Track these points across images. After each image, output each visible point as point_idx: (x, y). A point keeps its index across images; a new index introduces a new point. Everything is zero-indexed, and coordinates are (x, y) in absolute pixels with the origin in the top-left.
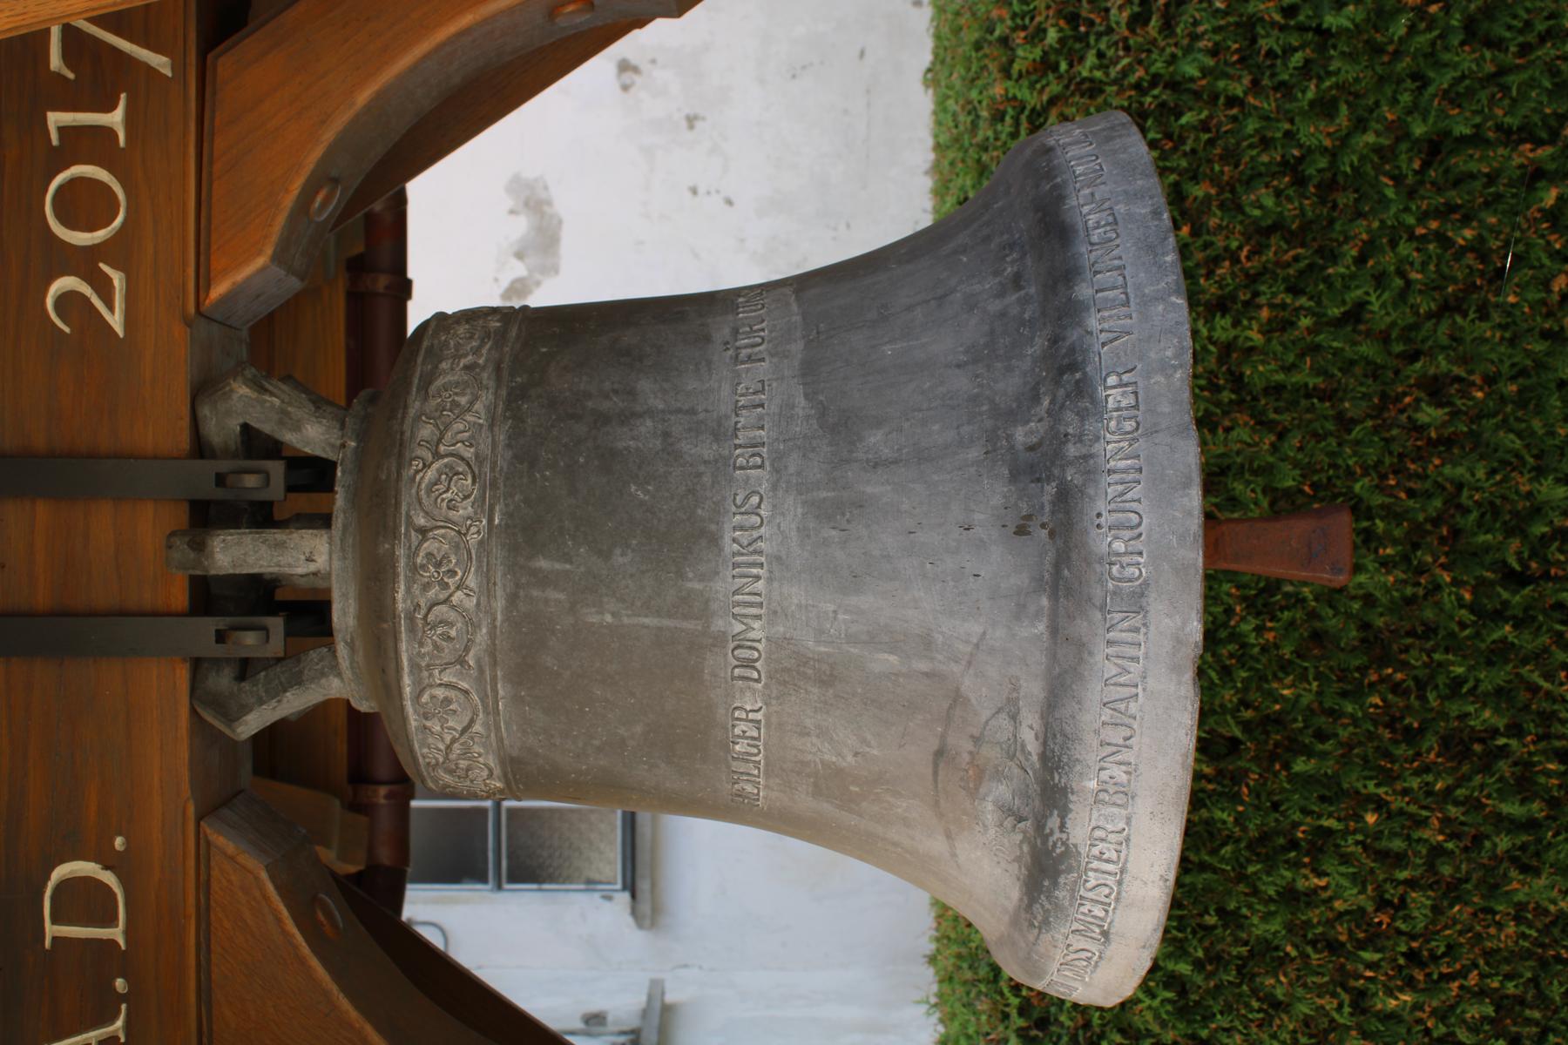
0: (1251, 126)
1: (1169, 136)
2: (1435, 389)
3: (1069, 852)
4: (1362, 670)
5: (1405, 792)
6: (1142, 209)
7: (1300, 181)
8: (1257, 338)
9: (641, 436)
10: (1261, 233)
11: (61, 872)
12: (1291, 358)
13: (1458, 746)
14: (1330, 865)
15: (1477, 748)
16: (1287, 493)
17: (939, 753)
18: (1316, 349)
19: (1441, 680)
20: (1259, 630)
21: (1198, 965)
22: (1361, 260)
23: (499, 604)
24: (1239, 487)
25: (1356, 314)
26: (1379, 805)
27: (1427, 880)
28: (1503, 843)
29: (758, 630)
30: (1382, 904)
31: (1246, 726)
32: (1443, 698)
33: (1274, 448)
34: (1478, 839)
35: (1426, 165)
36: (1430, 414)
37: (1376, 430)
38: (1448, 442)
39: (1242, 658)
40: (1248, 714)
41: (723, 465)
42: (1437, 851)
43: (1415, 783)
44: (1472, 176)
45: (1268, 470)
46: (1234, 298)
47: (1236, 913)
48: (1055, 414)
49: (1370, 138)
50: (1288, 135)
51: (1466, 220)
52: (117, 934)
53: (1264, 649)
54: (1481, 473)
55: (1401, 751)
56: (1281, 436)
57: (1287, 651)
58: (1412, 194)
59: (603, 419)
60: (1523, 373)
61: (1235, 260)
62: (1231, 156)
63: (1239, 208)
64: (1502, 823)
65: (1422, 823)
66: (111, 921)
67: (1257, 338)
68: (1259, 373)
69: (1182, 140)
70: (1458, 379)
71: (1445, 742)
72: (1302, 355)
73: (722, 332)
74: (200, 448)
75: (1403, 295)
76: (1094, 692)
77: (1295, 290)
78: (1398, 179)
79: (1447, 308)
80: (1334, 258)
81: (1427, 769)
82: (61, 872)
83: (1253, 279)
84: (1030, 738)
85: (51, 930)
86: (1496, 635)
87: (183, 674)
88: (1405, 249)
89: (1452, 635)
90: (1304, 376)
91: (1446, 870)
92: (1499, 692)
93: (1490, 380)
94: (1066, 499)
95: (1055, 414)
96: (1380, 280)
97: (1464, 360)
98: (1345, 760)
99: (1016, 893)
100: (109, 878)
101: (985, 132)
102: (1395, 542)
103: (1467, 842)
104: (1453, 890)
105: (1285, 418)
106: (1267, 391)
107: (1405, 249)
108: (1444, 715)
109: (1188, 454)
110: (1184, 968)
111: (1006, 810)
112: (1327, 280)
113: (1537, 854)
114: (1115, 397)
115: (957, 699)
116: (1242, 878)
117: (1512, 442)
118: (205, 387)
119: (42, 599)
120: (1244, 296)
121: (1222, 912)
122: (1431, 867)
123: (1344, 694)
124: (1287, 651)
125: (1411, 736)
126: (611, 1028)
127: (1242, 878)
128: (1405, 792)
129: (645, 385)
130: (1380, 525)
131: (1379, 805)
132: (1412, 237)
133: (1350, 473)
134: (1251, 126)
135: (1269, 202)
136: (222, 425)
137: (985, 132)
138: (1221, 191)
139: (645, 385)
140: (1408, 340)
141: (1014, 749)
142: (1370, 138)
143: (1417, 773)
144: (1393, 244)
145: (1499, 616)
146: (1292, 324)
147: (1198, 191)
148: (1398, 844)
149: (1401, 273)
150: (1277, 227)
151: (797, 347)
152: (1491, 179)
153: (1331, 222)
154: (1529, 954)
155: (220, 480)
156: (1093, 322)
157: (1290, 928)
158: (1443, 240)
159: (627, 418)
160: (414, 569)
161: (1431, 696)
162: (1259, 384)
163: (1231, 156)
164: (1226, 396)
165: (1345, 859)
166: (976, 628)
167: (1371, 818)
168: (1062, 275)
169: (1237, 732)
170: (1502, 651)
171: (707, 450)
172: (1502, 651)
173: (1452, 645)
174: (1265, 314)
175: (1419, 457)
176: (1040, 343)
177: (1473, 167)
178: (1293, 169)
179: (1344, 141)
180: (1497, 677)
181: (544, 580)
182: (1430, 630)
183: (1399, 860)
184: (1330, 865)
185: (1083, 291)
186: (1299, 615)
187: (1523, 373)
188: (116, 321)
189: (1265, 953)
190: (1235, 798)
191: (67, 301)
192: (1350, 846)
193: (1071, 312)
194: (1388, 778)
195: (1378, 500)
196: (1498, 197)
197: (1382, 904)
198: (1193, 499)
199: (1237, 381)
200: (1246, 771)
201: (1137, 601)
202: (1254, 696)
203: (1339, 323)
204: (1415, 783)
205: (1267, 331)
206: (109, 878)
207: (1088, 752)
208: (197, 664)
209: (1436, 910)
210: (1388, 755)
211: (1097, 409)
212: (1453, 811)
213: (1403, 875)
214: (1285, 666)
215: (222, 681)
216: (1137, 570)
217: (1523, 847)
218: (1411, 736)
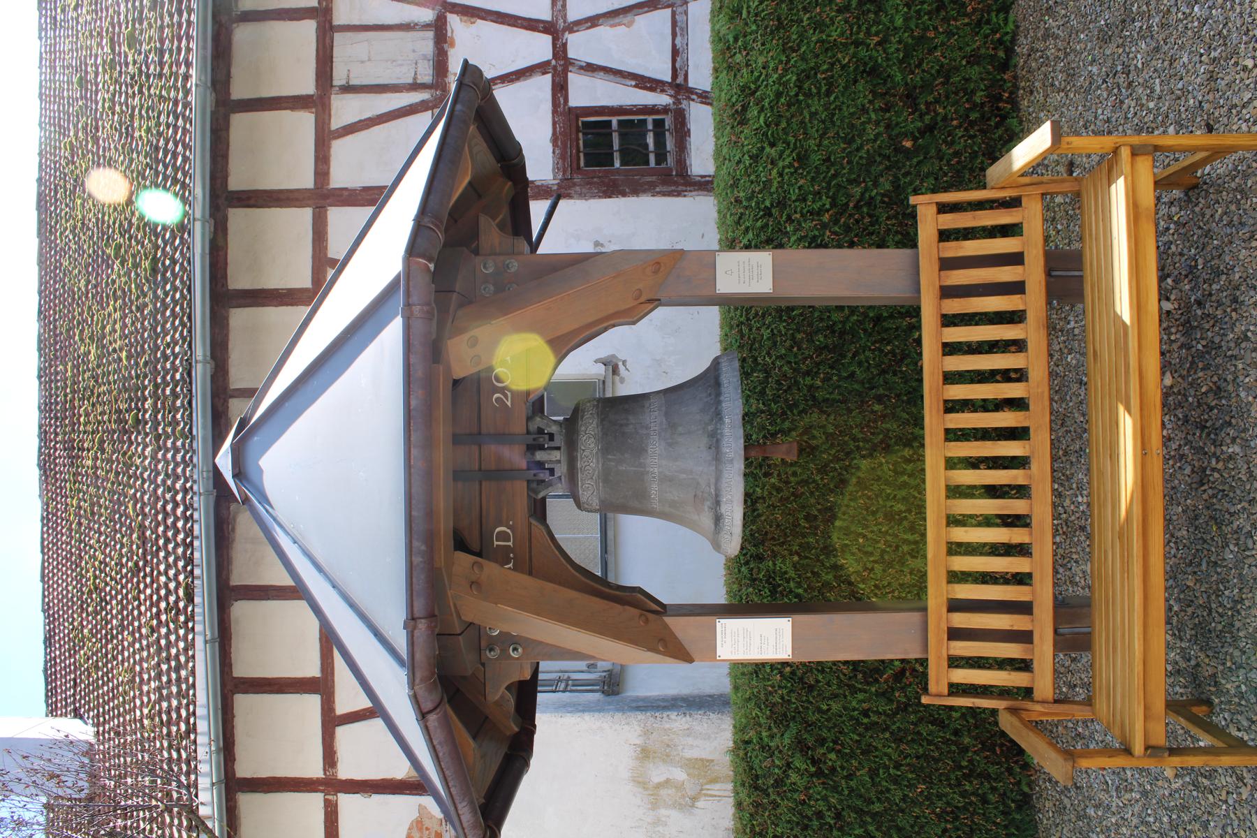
0: (816, 314)
1: (790, 318)
2: (879, 399)
3: (722, 515)
4: (857, 492)
5: (872, 532)
6: (735, 380)
7: (833, 332)
8: (819, 383)
9: (630, 429)
10: (820, 350)
11: (498, 529)
12: (831, 390)
13: (890, 516)
14: (848, 556)
15: (897, 517)
16: (831, 434)
17: (695, 496)
18: (839, 387)
19: (884, 494)
20: (822, 479)
21: (805, 590)
22: (854, 356)
23: (600, 465)
24: (815, 432)
25: (852, 374)
26: (864, 536)
27: (881, 561)
28: (906, 548)
29: (656, 470)
30: (866, 569)
31: (819, 511)
32: (884, 501)
33: (826, 419)
34: (897, 547)
35: (874, 326)
36: (877, 407)
37: (860, 413)
38: (884, 416)
39: (817, 488)
40: (819, 507)
41: (648, 435)
42: (883, 551)
43: (875, 529)
44: (891, 329)
45: (824, 427)
46: (811, 370)
47: (817, 573)
48: (716, 424)
49: (855, 318)
50: (829, 317)
51: (888, 344)
52: (510, 544)
53: (824, 485)
54: (895, 426)
55: (870, 518)
56: (828, 415)
57: (832, 486)
58: (870, 335)
59: (621, 425)
60: (909, 393)
61: (812, 358)
62: (810, 325)
63: (813, 341)
64: (906, 541)
65: (878, 542)
66: (509, 541)
67: (819, 383)
68: (820, 395)
69: (793, 319)
70: (887, 396)
71: (886, 515)
72: (834, 389)
73: (647, 405)
74: (528, 432)
75: (868, 368)
76: (724, 480)
77: (832, 368)
78: (865, 330)
79: (884, 372)
80: (844, 357)
81: (880, 524)
82: (498, 529)
83: (818, 364)
84: (712, 491)
85: (496, 543)
86: (902, 479)
87: (525, 483)
88: (867, 353)
89: (887, 480)
90: (836, 396)
91: (886, 557)
92: (904, 498)
93: (898, 396)
94: (718, 441)
95: (716, 424)
96: (860, 364)
97: (890, 389)
98: (852, 522)
99: (713, 526)
100: (509, 531)
101: (732, 314)
102: (867, 449)
103: (893, 548)
104: (890, 564)
105: (829, 410)
106: (824, 401)
107: (867, 353)
108: (885, 506)
109: (741, 432)
110: (800, 591)
111: (709, 507)
112: (842, 364)
113: (918, 552)
114: (727, 421)
115: (698, 483)
116: (818, 560)
117: (905, 416)
118: (529, 419)
119: (493, 467)
120: (815, 370)
121: (813, 573)
122: (882, 556)
123: (851, 500)
124: (832, 486)
125: (874, 513)
126: (599, 669)
127: (818, 560)
128: (872, 532)
129: (631, 417)
130: (861, 444)
131: (864, 536)
132: (870, 349)
133: (851, 427)
134: (816, 314)
135: (822, 339)
136: (533, 427)
137: (732, 314)
138: (807, 335)
139: (631, 417)
140: (869, 383)
141: (710, 494)
142: (855, 318)
143: (875, 525)
144: (864, 352)
145: (903, 473)
146: (831, 379)
147: (799, 336)
148: (870, 549)
149: (867, 362)
150: (826, 347)
151: (664, 408)
152: (897, 329)
153: (843, 345)
154: (916, 586)
155: (534, 440)
156: (723, 405)
157: (835, 577)
158: (881, 351)
159: (627, 425)
160: (582, 458)
161: (880, 500)
162: (820, 399)
163: (810, 325)
164: (810, 403)
165: (853, 554)
166: (701, 468)
167: (861, 540)
168: (719, 394)
169: (816, 513)
170: (904, 485)
171: (645, 432)
172: (904, 485)
173: (887, 483)
174: (822, 376)
175: (875, 421)
176: (713, 410)
177: (890, 326)
178: (831, 328)
179: (848, 318)
180: (903, 493)
181: (610, 460)
182: (879, 478)
183: (871, 554)
184: (848, 556)
185: (722, 398)
186: (836, 474)
187: (909, 393)
188: (509, 404)
189: (826, 585)
190: (816, 534)
191: (497, 399)
192: (854, 549)
193: (719, 402)
194: (865, 527)
195: (860, 436)
196: (899, 335)
197: (866, 569)
198: (742, 441)
199: (814, 398)
200: (819, 526)
201: (731, 461)
202: (821, 501)
203: (847, 378)
204: (875, 529)
205: (823, 381)
206: (509, 531)
207: (723, 493)
208: (528, 481)
209: (884, 571)
210: (866, 520)
211: (724, 422)
212: (889, 538)
213: (872, 559)
214: (832, 491)
215: (534, 485)
216: (732, 455)
217: (912, 550)
218: (874, 513)
